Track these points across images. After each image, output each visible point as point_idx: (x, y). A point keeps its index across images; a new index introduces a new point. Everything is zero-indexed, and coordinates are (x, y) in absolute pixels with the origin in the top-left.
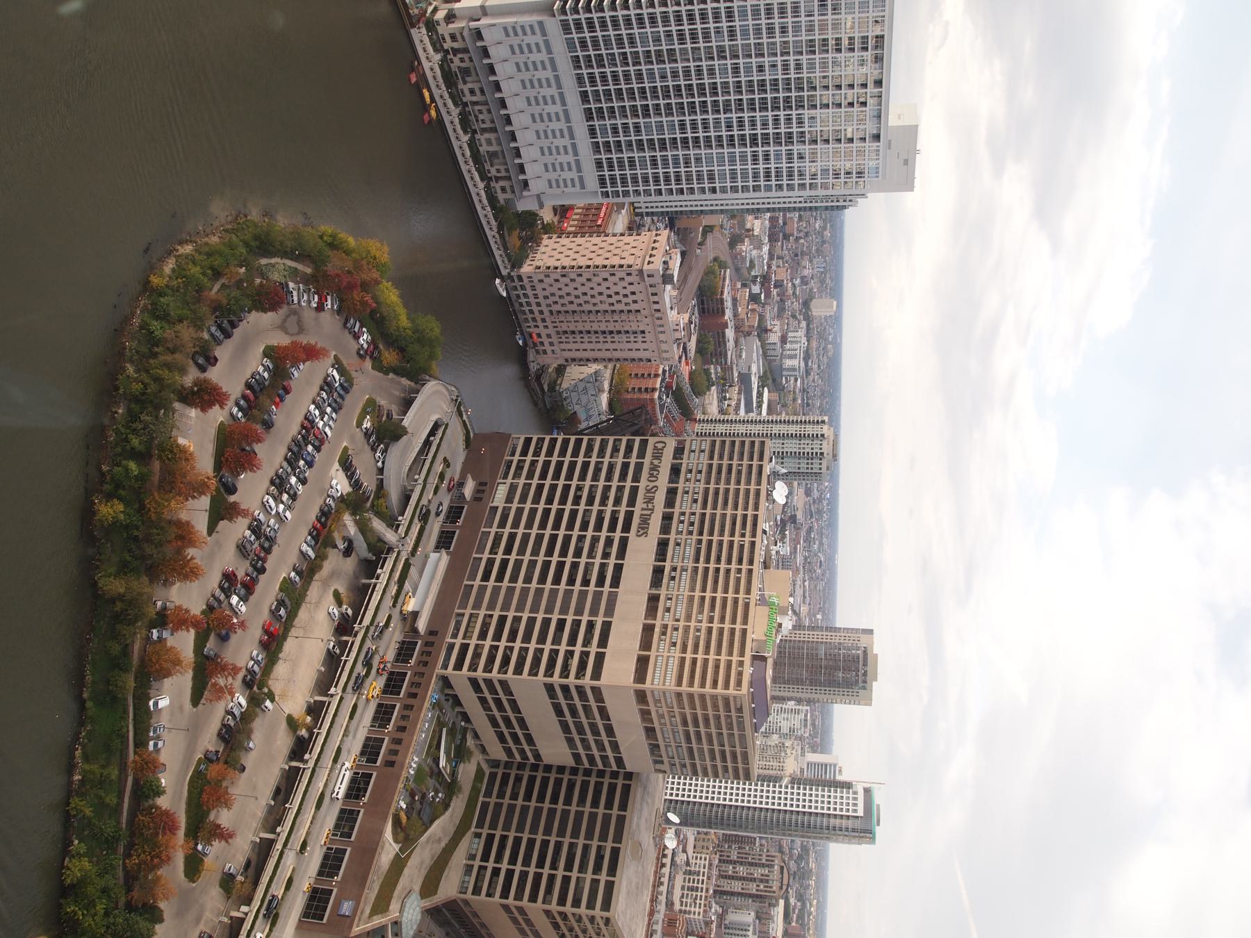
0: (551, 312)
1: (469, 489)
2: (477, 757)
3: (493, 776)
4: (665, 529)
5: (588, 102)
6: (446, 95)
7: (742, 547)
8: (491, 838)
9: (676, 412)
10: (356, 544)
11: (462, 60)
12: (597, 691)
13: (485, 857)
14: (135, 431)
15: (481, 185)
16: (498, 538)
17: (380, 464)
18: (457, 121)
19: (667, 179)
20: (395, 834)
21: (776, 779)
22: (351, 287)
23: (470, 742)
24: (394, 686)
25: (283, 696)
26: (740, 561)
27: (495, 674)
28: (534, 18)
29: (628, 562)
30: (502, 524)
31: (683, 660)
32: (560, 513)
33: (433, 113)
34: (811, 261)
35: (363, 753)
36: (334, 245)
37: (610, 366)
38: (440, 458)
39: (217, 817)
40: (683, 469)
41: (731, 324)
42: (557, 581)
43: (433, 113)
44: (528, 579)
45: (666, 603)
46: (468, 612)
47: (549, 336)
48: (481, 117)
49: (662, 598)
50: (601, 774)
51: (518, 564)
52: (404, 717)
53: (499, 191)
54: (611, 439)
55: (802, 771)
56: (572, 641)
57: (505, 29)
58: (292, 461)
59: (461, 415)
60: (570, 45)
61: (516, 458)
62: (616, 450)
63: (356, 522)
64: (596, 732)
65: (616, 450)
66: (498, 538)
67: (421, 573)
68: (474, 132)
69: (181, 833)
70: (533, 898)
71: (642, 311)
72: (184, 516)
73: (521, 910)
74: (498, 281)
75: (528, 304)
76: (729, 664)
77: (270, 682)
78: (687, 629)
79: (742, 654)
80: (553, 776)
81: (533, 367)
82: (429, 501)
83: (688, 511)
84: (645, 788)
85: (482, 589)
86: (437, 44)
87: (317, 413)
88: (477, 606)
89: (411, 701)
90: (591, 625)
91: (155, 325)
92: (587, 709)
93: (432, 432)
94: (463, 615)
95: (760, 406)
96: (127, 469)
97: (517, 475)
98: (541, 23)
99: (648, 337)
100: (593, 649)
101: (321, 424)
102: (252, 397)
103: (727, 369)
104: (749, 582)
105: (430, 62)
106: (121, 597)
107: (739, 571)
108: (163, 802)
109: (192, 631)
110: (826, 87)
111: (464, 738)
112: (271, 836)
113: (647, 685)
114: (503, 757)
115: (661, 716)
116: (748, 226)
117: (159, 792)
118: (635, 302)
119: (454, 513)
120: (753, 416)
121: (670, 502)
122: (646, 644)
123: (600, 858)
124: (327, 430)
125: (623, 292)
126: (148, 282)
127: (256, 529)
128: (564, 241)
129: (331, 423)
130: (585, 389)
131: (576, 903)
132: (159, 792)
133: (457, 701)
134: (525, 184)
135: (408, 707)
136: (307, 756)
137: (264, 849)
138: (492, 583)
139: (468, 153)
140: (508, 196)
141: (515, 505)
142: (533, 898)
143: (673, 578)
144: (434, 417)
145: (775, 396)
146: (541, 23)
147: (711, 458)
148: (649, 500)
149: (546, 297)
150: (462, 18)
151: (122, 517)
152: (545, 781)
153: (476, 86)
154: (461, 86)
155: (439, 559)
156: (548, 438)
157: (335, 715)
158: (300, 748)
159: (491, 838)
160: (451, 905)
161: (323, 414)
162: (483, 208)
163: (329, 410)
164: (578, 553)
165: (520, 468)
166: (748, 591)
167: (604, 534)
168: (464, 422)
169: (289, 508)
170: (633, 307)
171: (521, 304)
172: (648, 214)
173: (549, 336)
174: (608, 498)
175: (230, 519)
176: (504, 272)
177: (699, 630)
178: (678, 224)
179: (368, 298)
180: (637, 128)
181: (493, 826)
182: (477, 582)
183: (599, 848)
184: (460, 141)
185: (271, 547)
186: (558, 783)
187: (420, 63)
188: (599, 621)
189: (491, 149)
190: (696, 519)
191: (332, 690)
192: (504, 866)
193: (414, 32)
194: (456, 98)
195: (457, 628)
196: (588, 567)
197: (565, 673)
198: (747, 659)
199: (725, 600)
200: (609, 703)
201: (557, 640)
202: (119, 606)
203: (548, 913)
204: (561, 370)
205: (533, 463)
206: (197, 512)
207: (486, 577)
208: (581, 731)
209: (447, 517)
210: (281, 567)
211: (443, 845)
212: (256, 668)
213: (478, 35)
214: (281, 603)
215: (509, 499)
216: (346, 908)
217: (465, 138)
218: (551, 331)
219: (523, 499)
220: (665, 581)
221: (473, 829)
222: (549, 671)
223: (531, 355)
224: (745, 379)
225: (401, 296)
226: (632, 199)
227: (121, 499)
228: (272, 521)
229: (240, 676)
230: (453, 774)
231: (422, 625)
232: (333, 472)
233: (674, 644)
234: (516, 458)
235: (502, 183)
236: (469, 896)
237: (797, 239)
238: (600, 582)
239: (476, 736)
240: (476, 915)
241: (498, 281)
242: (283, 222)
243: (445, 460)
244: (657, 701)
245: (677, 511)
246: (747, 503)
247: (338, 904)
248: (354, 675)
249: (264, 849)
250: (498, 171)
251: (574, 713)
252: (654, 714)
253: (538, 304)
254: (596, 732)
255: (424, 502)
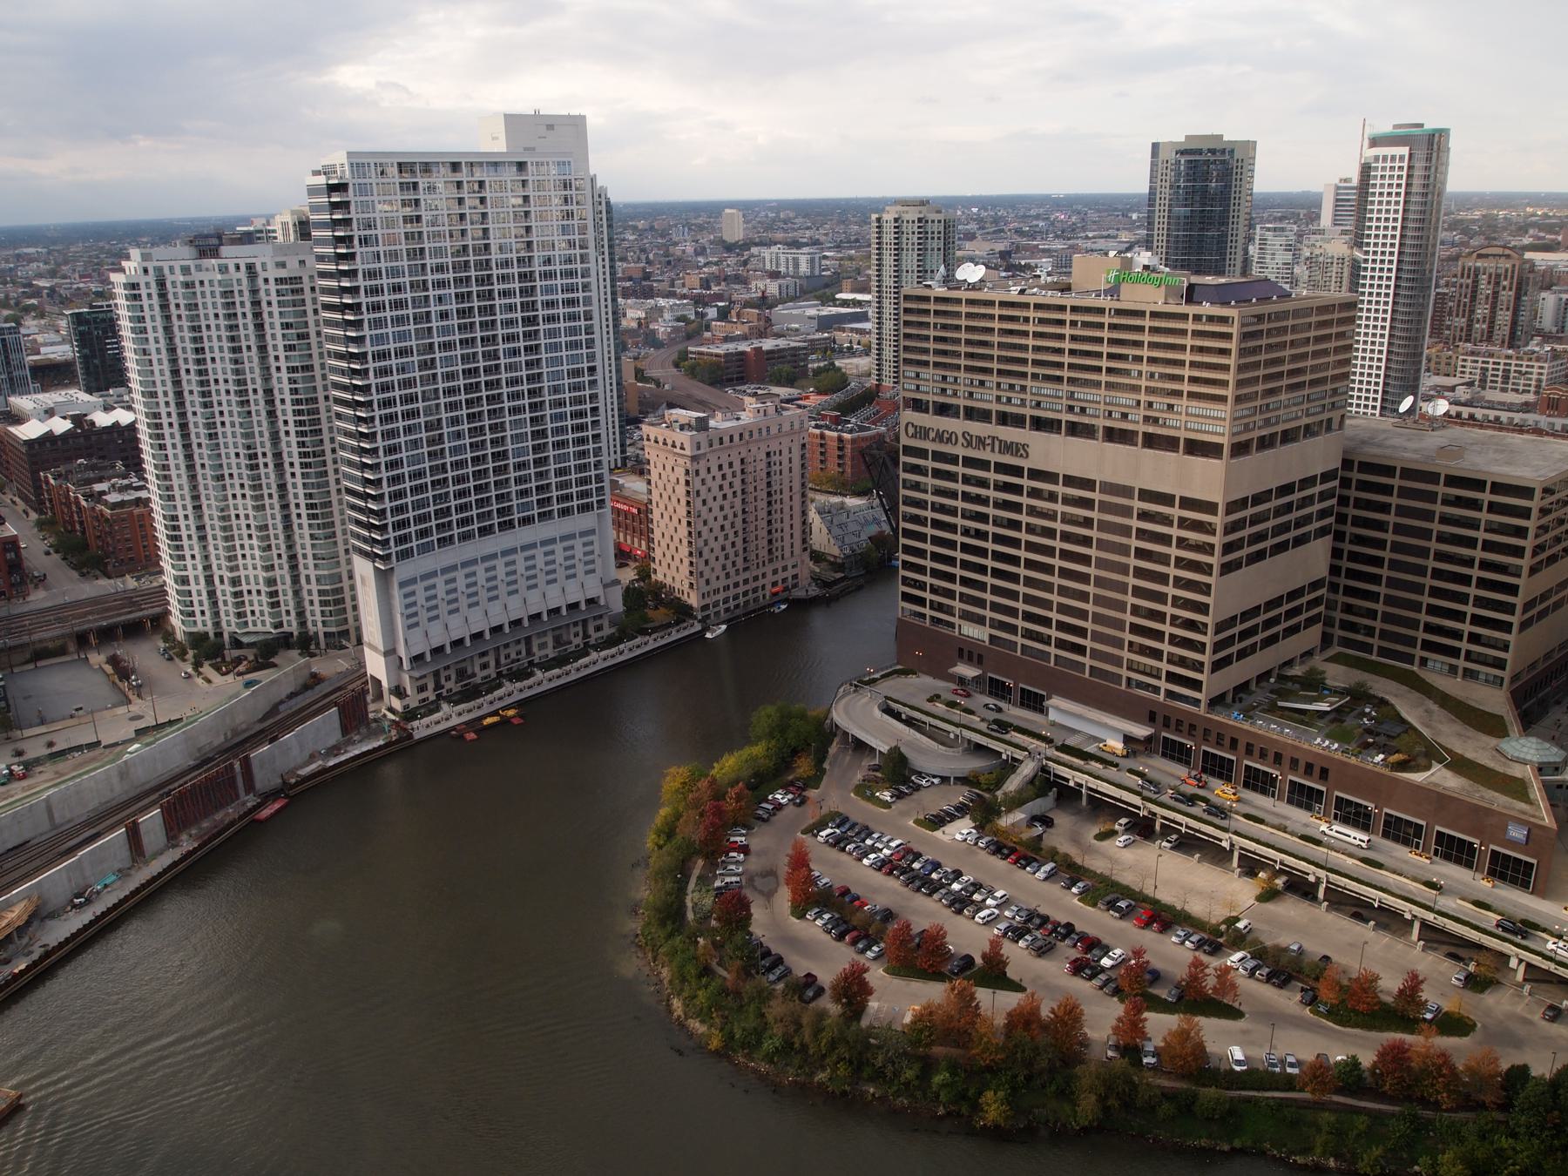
0: (746, 569)
1: (968, 671)
2: (1317, 661)
3: (1346, 643)
4: (1018, 421)
5: (491, 526)
6: (489, 697)
7: (1042, 321)
8: (1427, 646)
9: (868, 411)
10: (1037, 812)
11: (448, 678)
12: (1232, 507)
13: (1454, 653)
14: (896, 1074)
15: (594, 655)
16: (1029, 634)
17: (936, 781)
18: (519, 685)
19: (581, 428)
20: (1418, 769)
21: (1356, 268)
22: (719, 812)
23: (1297, 671)
24: (1222, 767)
25: (1232, 906)
26: (1061, 323)
27: (1208, 639)
28: (396, 593)
29: (1061, 469)
30: (1012, 629)
31: (1191, 395)
32: (998, 556)
33: (511, 713)
34: (676, 244)
35: (1309, 808)
36: (669, 832)
37: (811, 495)
38: (928, 707)
39: (1389, 993)
40: (941, 399)
41: (756, 344)
42: (1085, 560)
43: (511, 713)
44: (1084, 596)
45: (1115, 419)
46: (1125, 673)
47: (775, 572)
48: (513, 656)
49: (1109, 423)
50: (1343, 501)
51: (1063, 609)
52: (1263, 755)
53: (600, 634)
54: (903, 492)
55: (1344, 233)
56: (1165, 539)
57: (410, 627)
58: (933, 888)
59: (874, 681)
60: (425, 549)
61: (927, 611)
62: (916, 486)
63: (1009, 811)
64: (1288, 508)
65: (916, 486)
66: (1029, 634)
67: (1073, 731)
68: (531, 663)
69: (1408, 1038)
70: (1512, 590)
71: (742, 456)
72: (1000, 1021)
73: (1528, 606)
74: (708, 635)
75: (736, 597)
76: (1196, 334)
77: (1214, 921)
78: (1150, 390)
79: (1184, 317)
80: (1345, 564)
81: (814, 591)
82: (983, 720)
83: (995, 392)
84: (1363, 442)
85: (1095, 654)
86: (430, 708)
87: (872, 856)
88: (1117, 661)
89: (1241, 747)
90: (1144, 515)
91: (768, 1045)
92: (1255, 520)
93: (896, 715)
94: (1129, 679)
95: (859, 303)
96: (943, 1085)
97: (949, 610)
98: (402, 585)
99: (774, 447)
100: (1176, 512)
101: (886, 852)
102: (855, 934)
103: (813, 346)
104: (1088, 310)
105: (450, 716)
106: (1102, 1099)
107: (1074, 324)
108: (1367, 1059)
109: (1146, 1015)
110: (463, 232)
111: (1293, 679)
112: (1417, 925)
113: (1225, 441)
114: (1316, 631)
115: (1267, 422)
116: (634, 325)
117: (1354, 1063)
118: (731, 465)
119: (998, 689)
120: (872, 312)
121: (984, 416)
122: (1170, 444)
123: (1459, 502)
124: (893, 844)
125: (719, 480)
126: (717, 1053)
127: (1017, 933)
128: (658, 554)
129: (885, 839)
130: (840, 526)
131: (1521, 532)
132: (1354, 1063)
133: (1243, 688)
134: (591, 602)
135: (1249, 750)
136: (1312, 879)
137: (1433, 936)
138: (1087, 643)
139: (556, 671)
140: (606, 623)
141: (988, 613)
142: (1512, 590)
143: (1083, 410)
144: (877, 713)
145: (847, 284)
146: (402, 585)
147: (926, 364)
148: (981, 442)
149: (728, 576)
150: (399, 678)
151: (1001, 1094)
152: (1351, 574)
153: (478, 662)
154: (478, 680)
155: (1057, 708)
156: (902, 572)
157: (1258, 842)
158: (1301, 888)
159: (1427, 646)
160: (1520, 697)
161: (873, 849)
162: (621, 653)
163: (869, 842)
164: (1050, 533)
165: (940, 607)
166: (1101, 311)
167: (1024, 500)
168: (883, 677)
169: (991, 893)
170: (737, 467)
171: (737, 606)
172: (623, 452)
173: (775, 572)
174: (978, 496)
175: (1005, 964)
176: (698, 627)
177: (1152, 375)
178: (634, 413)
179: (732, 792)
180: (521, 466)
181: (1411, 642)
182: (1087, 661)
183: (1445, 502)
184: (543, 681)
185: (1039, 916)
186: (1354, 557)
187: (453, 728)
188: (1137, 505)
189: (550, 644)
190: (1005, 381)
191: (1225, 844)
192: (1466, 628)
193: (417, 735)
194: (493, 685)
195: (1147, 687)
196: (1067, 519)
197: (1207, 549)
198: (1191, 310)
199: (1112, 342)
200: (1248, 492)
201: (1164, 559)
202: (1112, 1102)
203: (1533, 570)
204: (817, 557)
205: (934, 590)
206: (995, 1004)
207: (1080, 650)
208: (1285, 528)
209: (1003, 698)
210: (1066, 904)
211: (1435, 707)
212: (1195, 938)
213: (417, 659)
214: (1111, 905)
215: (980, 620)
216: (1517, 833)
217: (539, 674)
218: (769, 569)
219: (981, 603)
220: (1086, 420)
221: (1415, 668)
222: (1206, 569)
223: (798, 593)
224: (825, 323)
225: (731, 751)
226: (605, 471)
227: (980, 1093)
228: (1007, 913)
229: (1205, 958)
230: (1336, 692)
231: (1141, 731)
232: (946, 838)
233: (1171, 407)
234: (927, 611)
235: (591, 630)
236: (1506, 675)
237: (649, 262)
238: (1087, 504)
239: (1289, 663)
240: (1533, 666)
241: (708, 635)
242: (644, 891)
243: (930, 700)
244: (1247, 428)
245: (994, 407)
246: (984, 316)
247: (1512, 844)
248: (1206, 816)
249: (1433, 936)
250: (576, 635)
251: (1260, 537)
252: (1264, 432)
253: (736, 585)
254: (1288, 508)
255: (983, 727)
